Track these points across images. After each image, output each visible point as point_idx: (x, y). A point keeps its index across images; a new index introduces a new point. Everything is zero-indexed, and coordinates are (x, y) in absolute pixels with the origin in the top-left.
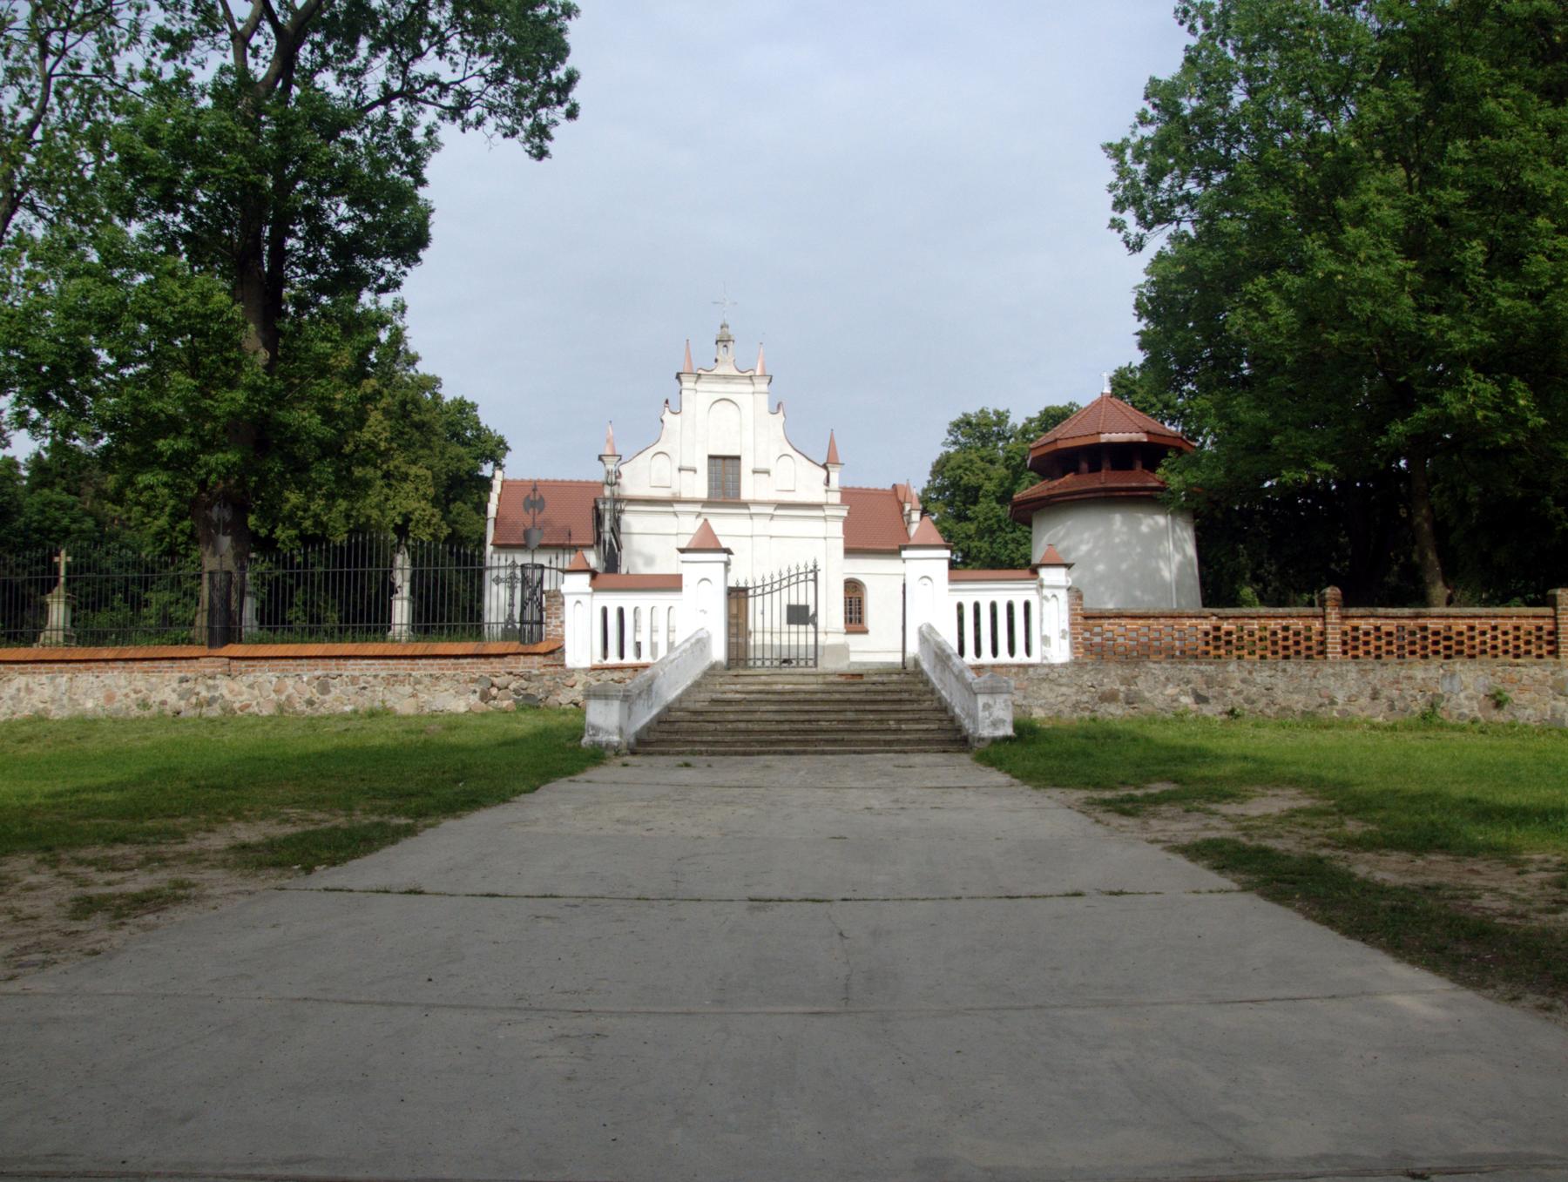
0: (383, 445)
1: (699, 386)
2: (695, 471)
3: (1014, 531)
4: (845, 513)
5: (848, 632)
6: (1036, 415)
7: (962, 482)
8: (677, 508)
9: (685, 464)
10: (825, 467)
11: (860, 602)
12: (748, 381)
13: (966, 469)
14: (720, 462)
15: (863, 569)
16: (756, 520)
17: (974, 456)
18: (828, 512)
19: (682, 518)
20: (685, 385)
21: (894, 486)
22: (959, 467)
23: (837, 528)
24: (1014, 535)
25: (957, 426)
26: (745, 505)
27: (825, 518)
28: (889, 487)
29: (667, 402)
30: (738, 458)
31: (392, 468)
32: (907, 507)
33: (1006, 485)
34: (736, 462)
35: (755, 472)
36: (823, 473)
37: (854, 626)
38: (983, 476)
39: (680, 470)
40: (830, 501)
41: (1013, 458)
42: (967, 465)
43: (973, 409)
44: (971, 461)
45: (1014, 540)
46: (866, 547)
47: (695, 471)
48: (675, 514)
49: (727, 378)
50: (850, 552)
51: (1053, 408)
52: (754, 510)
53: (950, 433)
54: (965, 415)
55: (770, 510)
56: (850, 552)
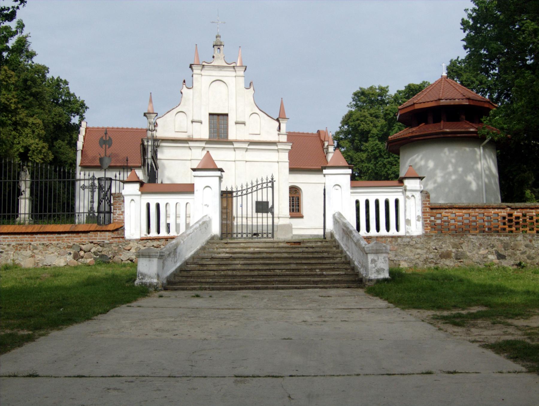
0: (13, 106)
1: (203, 72)
2: (201, 123)
3: (389, 157)
4: (289, 148)
5: (292, 217)
6: (403, 89)
7: (360, 128)
8: (191, 144)
9: (196, 119)
10: (278, 120)
11: (298, 199)
12: (232, 69)
13: (362, 121)
14: (216, 117)
15: (300, 180)
16: (238, 151)
17: (366, 114)
18: (280, 147)
19: (193, 150)
20: (195, 71)
21: (318, 131)
22: (358, 120)
23: (285, 156)
24: (389, 160)
25: (355, 94)
26: (231, 143)
27: (278, 150)
28: (315, 132)
29: (184, 82)
30: (227, 115)
31: (18, 119)
32: (326, 144)
33: (385, 130)
34: (225, 117)
35: (236, 123)
36: (277, 124)
37: (295, 214)
38: (372, 125)
39: (192, 122)
40: (281, 140)
41: (389, 114)
42: (362, 118)
43: (366, 86)
44: (365, 116)
45: (389, 162)
46: (302, 167)
47: (201, 123)
48: (190, 148)
49: (220, 67)
50: (293, 170)
51: (413, 85)
52: (236, 145)
53: (353, 98)
54: (361, 89)
55: (246, 146)
56: (293, 170)
